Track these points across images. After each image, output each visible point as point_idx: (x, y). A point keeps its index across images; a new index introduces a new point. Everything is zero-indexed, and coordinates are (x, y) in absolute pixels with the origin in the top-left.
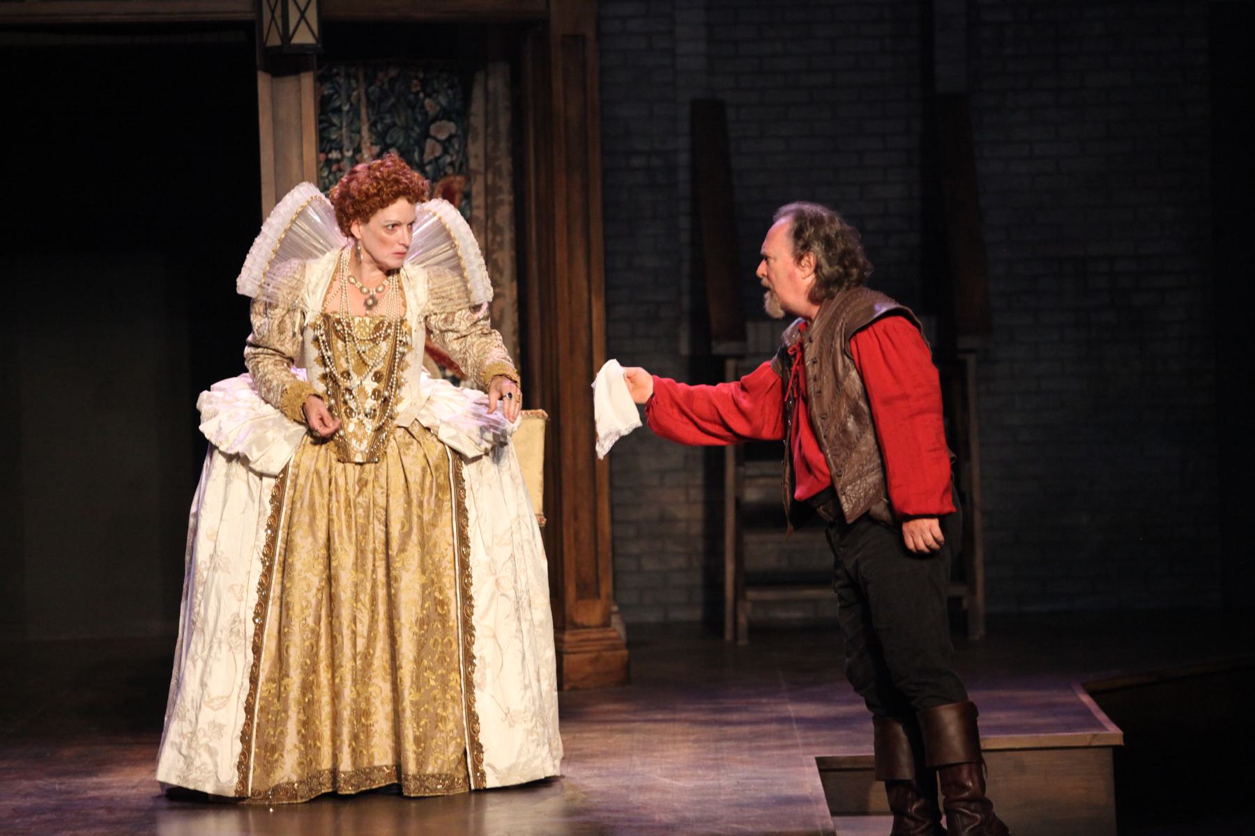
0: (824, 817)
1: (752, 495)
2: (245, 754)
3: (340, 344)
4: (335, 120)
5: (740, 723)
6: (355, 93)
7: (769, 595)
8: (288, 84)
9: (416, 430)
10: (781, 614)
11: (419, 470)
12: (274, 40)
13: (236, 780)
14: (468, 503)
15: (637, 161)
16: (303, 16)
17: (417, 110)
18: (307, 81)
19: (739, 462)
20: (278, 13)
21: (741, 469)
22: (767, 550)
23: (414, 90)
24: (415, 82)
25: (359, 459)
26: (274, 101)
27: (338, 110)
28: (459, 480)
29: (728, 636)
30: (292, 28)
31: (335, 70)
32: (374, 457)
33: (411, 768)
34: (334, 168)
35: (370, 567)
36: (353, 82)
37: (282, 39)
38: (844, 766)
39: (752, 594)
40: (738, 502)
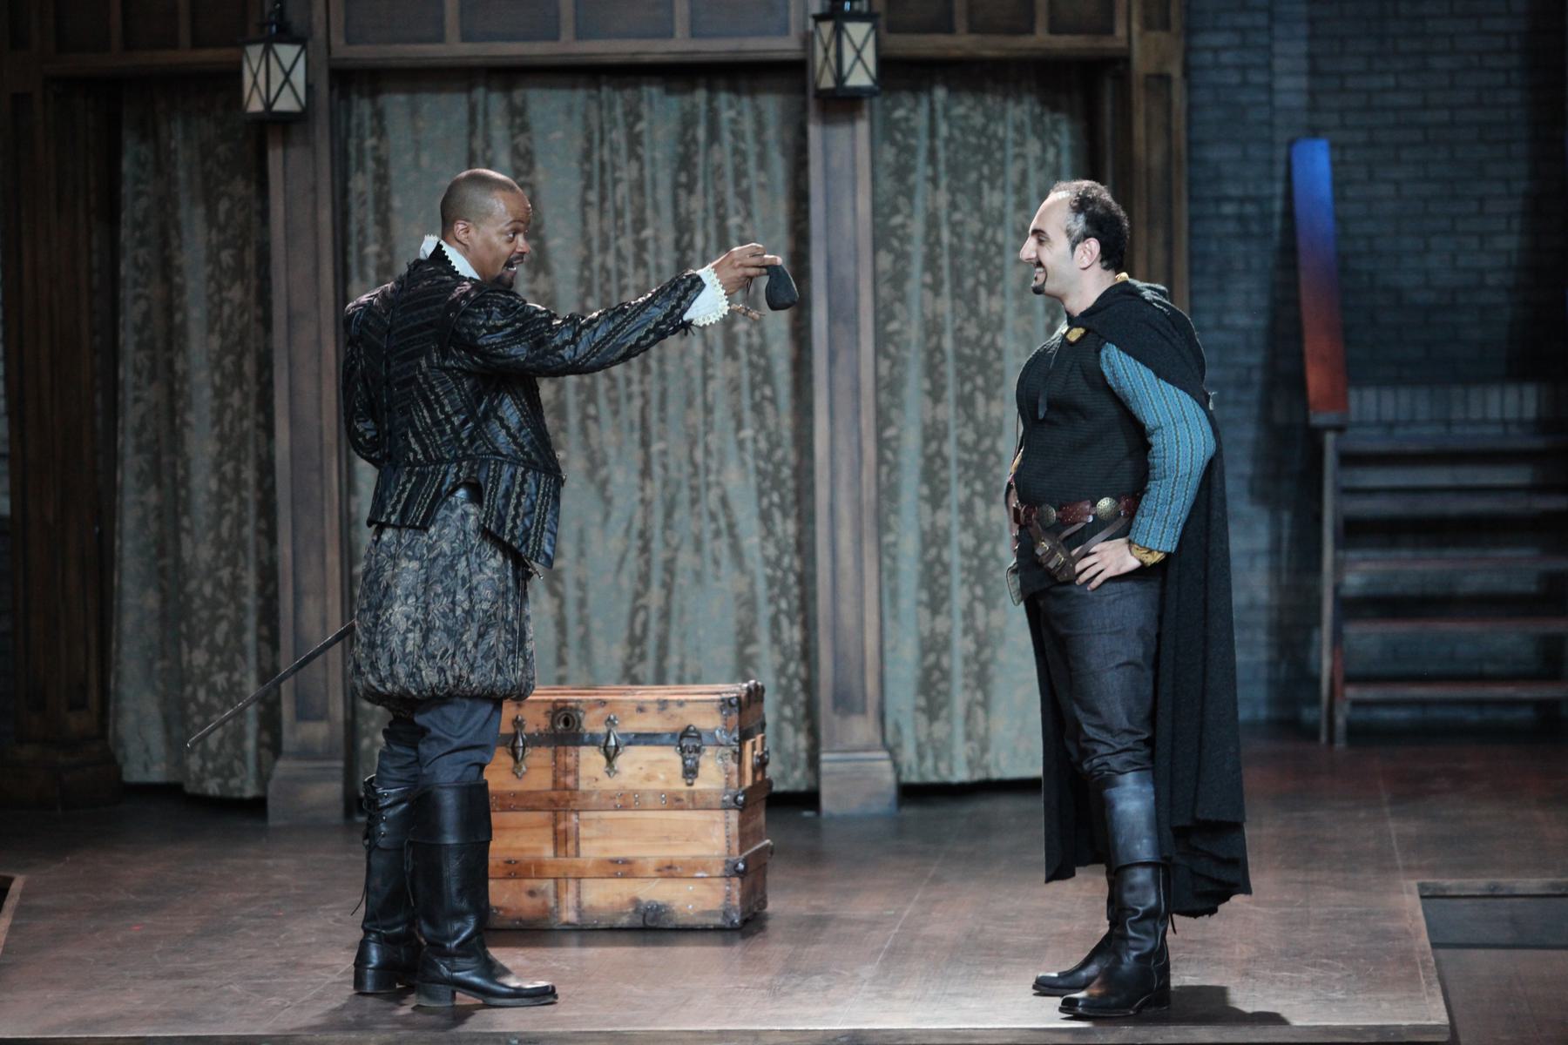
0: (1424, 953)
1: (1354, 581)
7: (1371, 693)
8: (841, 133)
10: (1386, 714)
12: (827, 82)
15: (1228, 209)
19: (1339, 544)
20: (832, 52)
22: (1368, 636)
29: (1323, 738)
30: (272, 95)
39: (1352, 692)
40: (1337, 588)
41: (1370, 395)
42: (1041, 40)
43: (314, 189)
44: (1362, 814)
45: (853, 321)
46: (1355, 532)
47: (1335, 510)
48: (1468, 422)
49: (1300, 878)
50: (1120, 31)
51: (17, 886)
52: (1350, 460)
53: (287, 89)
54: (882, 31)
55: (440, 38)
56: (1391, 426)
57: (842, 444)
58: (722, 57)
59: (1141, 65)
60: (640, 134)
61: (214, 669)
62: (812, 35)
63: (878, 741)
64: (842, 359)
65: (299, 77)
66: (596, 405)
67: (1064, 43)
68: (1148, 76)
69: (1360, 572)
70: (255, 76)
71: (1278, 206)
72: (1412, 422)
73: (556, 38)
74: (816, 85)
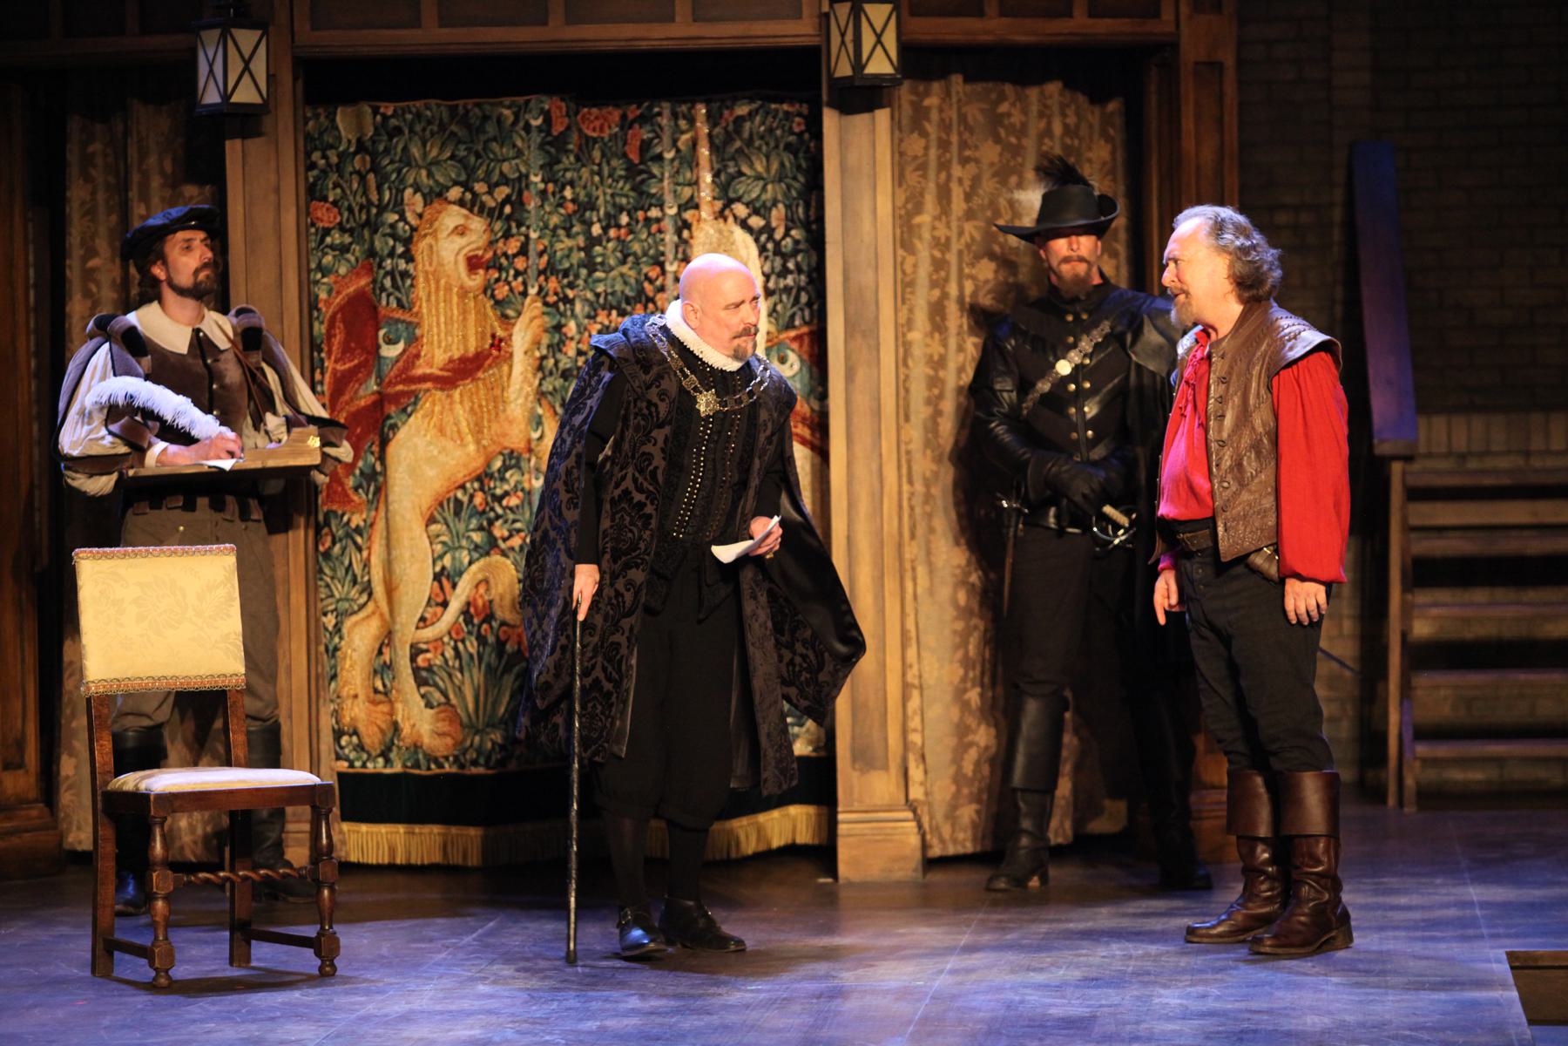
1: (1422, 629)
4: (656, 170)
5: (1409, 908)
6: (685, 137)
7: (1443, 750)
8: (861, 120)
10: (1456, 775)
12: (844, 69)
16: (879, 41)
17: (801, 155)
19: (1407, 588)
20: (849, 37)
21: (1409, 597)
22: (1440, 694)
23: (797, 130)
24: (797, 119)
26: (842, 143)
27: (659, 158)
29: (1392, 801)
31: (656, 110)
34: (654, 228)
36: (683, 124)
37: (853, 68)
38: (1540, 964)
39: (1422, 749)
40: (1404, 636)
41: (1439, 422)
42: (1079, 24)
43: (277, 190)
44: (1439, 881)
45: (873, 333)
46: (1425, 573)
47: (1404, 551)
48: (1548, 452)
50: (1167, 15)
52: (1416, 494)
53: (246, 78)
54: (905, 13)
55: (416, 23)
56: (1463, 457)
57: (861, 471)
58: (727, 44)
59: (1191, 51)
60: (928, 109)
62: (827, 15)
63: (903, 801)
64: (861, 374)
65: (259, 67)
67: (1104, 27)
68: (1197, 63)
69: (1426, 617)
70: (211, 65)
71: (1338, 214)
72: (1486, 453)
73: (1070, 15)
74: (830, 75)
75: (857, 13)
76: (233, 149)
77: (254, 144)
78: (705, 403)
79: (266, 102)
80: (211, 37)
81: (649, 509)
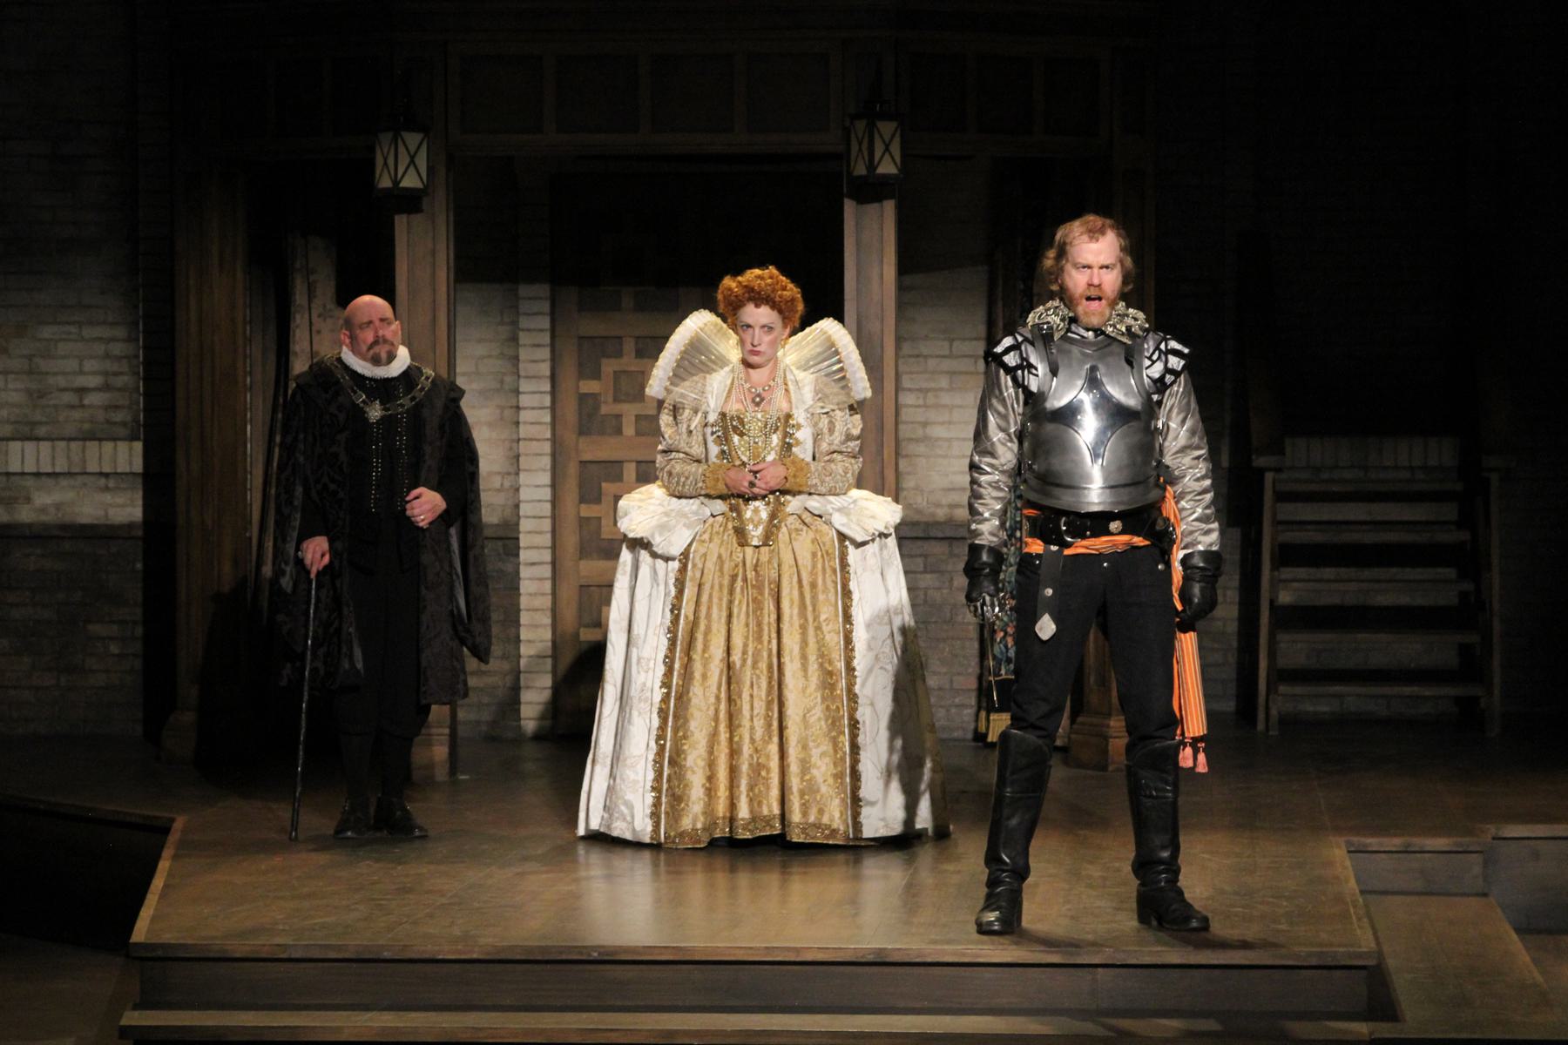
1: (1285, 598)
2: (657, 804)
3: (736, 438)
7: (1298, 690)
8: (873, 208)
9: (807, 517)
10: (1309, 707)
11: (809, 556)
12: (860, 170)
13: (650, 828)
14: (853, 586)
16: (887, 149)
18: (889, 207)
22: (1297, 648)
25: (755, 543)
28: (844, 564)
29: (1261, 726)
32: (768, 538)
33: (796, 817)
35: (766, 638)
39: (1282, 689)
40: (1272, 602)
43: (434, 253)
46: (1288, 555)
49: (39, 551)
51: (178, 824)
52: (1282, 497)
61: (1006, 812)
66: (1122, 533)
69: (1289, 588)
70: (385, 159)
74: (849, 173)
75: (871, 129)
76: (400, 222)
77: (417, 219)
78: (375, 413)
79: (426, 187)
80: (385, 138)
81: (341, 495)
